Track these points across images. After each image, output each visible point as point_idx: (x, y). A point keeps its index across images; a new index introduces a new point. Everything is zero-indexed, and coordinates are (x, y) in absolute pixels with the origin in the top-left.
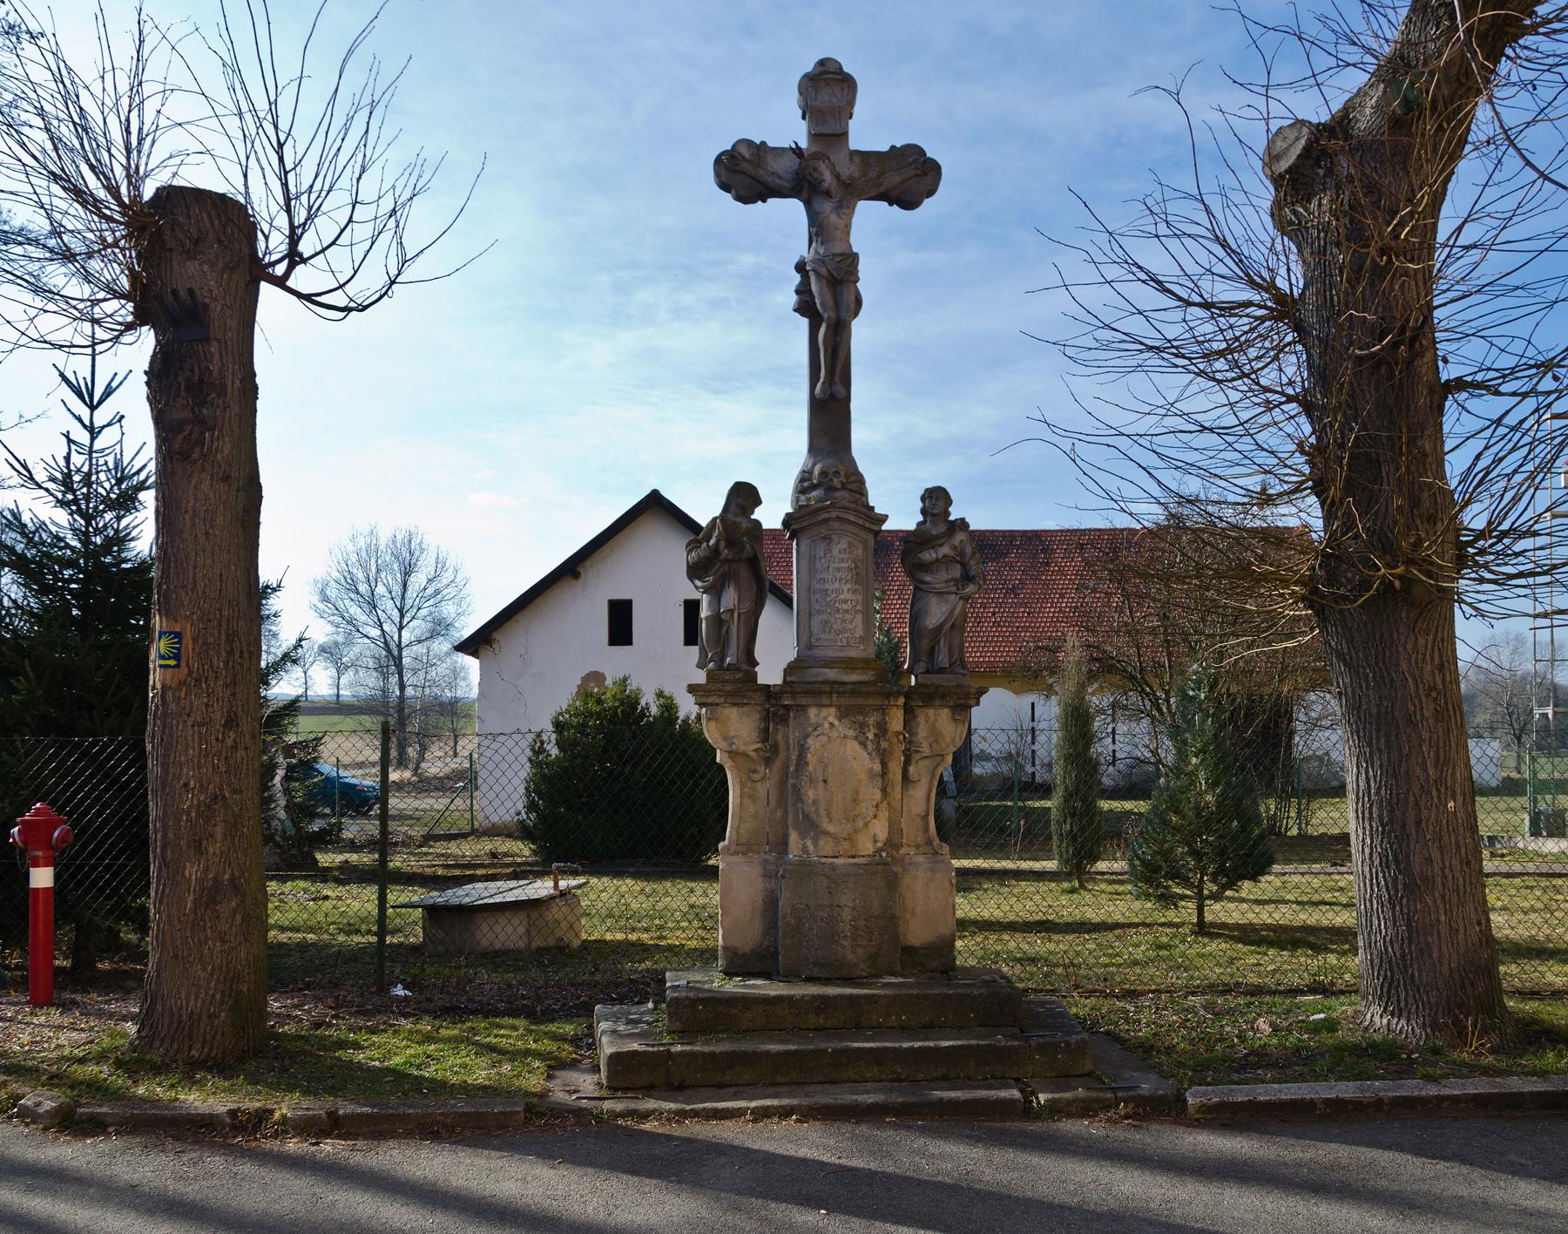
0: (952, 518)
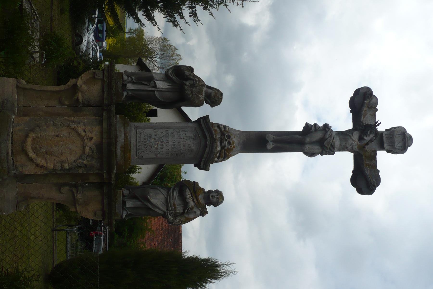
0: (207, 207)
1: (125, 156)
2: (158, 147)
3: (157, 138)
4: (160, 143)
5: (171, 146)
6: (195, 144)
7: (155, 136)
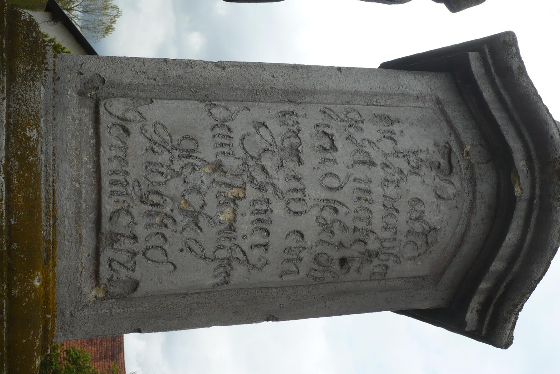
1: (15, 292)
2: (239, 218)
3: (230, 163)
4: (251, 193)
5: (315, 212)
6: (445, 196)
7: (222, 145)
